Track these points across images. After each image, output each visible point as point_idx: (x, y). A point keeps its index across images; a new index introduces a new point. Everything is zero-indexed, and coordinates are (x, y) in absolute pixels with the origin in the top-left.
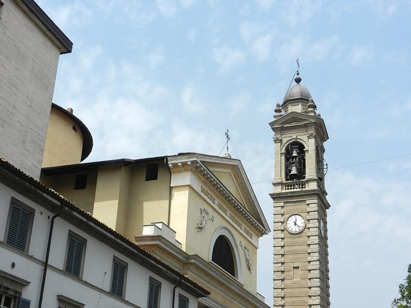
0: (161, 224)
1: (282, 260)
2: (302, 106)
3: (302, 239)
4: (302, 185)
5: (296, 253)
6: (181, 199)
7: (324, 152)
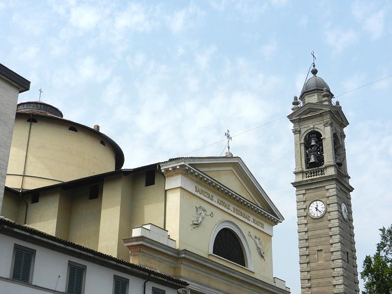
0: (150, 225)
2: (318, 96)
3: (324, 223)
4: (322, 172)
5: (319, 237)
6: (174, 200)
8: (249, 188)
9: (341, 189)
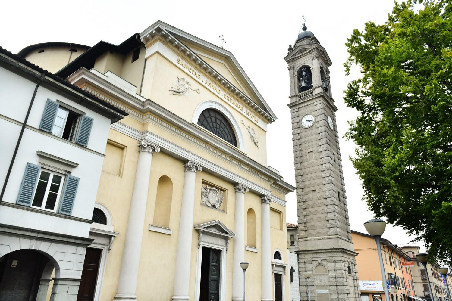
1: (300, 149)
7: (329, 73)
8: (243, 85)
9: (327, 105)
